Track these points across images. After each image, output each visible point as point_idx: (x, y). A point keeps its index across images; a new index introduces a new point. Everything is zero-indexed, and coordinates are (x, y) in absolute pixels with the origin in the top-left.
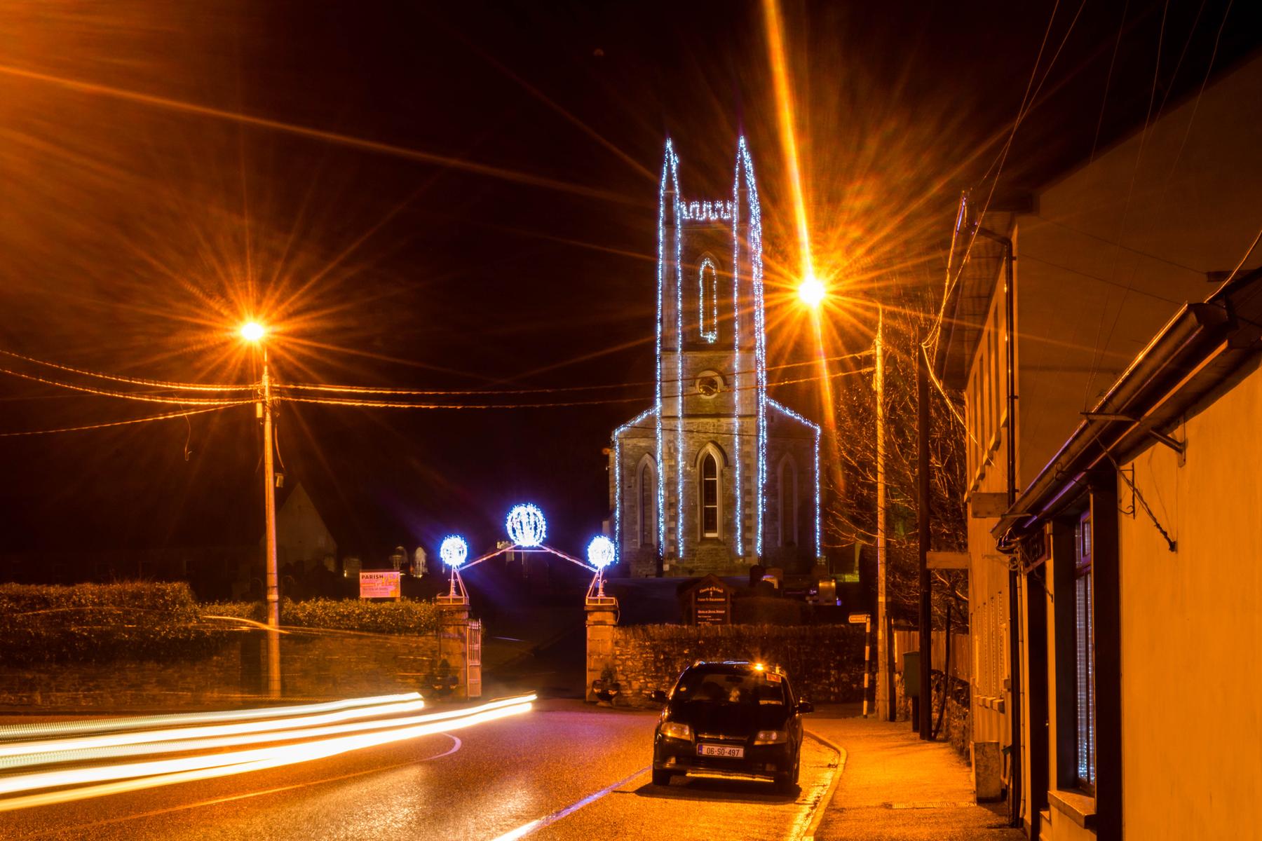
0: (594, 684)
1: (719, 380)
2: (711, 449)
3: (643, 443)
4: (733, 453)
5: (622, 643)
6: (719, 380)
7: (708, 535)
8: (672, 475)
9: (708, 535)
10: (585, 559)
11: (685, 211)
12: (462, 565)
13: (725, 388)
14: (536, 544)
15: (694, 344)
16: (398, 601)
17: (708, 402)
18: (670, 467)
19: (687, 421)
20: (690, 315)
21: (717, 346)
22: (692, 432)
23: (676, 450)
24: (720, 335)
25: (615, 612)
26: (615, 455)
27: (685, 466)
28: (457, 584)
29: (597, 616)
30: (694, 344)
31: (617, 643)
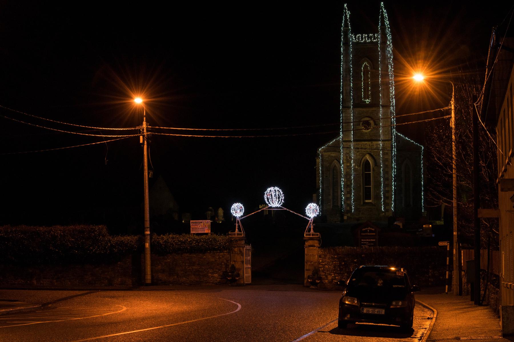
0: (309, 277)
1: (367, 119)
2: (368, 157)
3: (333, 154)
5: (323, 256)
6: (367, 119)
7: (367, 201)
8: (348, 170)
9: (367, 201)
10: (304, 213)
12: (242, 216)
13: (375, 126)
14: (279, 206)
15: (359, 104)
16: (209, 235)
17: (366, 133)
18: (347, 166)
19: (356, 143)
21: (370, 105)
23: (350, 158)
24: (372, 100)
25: (319, 240)
26: (319, 161)
27: (355, 166)
28: (239, 226)
29: (310, 242)
30: (359, 104)
31: (320, 256)
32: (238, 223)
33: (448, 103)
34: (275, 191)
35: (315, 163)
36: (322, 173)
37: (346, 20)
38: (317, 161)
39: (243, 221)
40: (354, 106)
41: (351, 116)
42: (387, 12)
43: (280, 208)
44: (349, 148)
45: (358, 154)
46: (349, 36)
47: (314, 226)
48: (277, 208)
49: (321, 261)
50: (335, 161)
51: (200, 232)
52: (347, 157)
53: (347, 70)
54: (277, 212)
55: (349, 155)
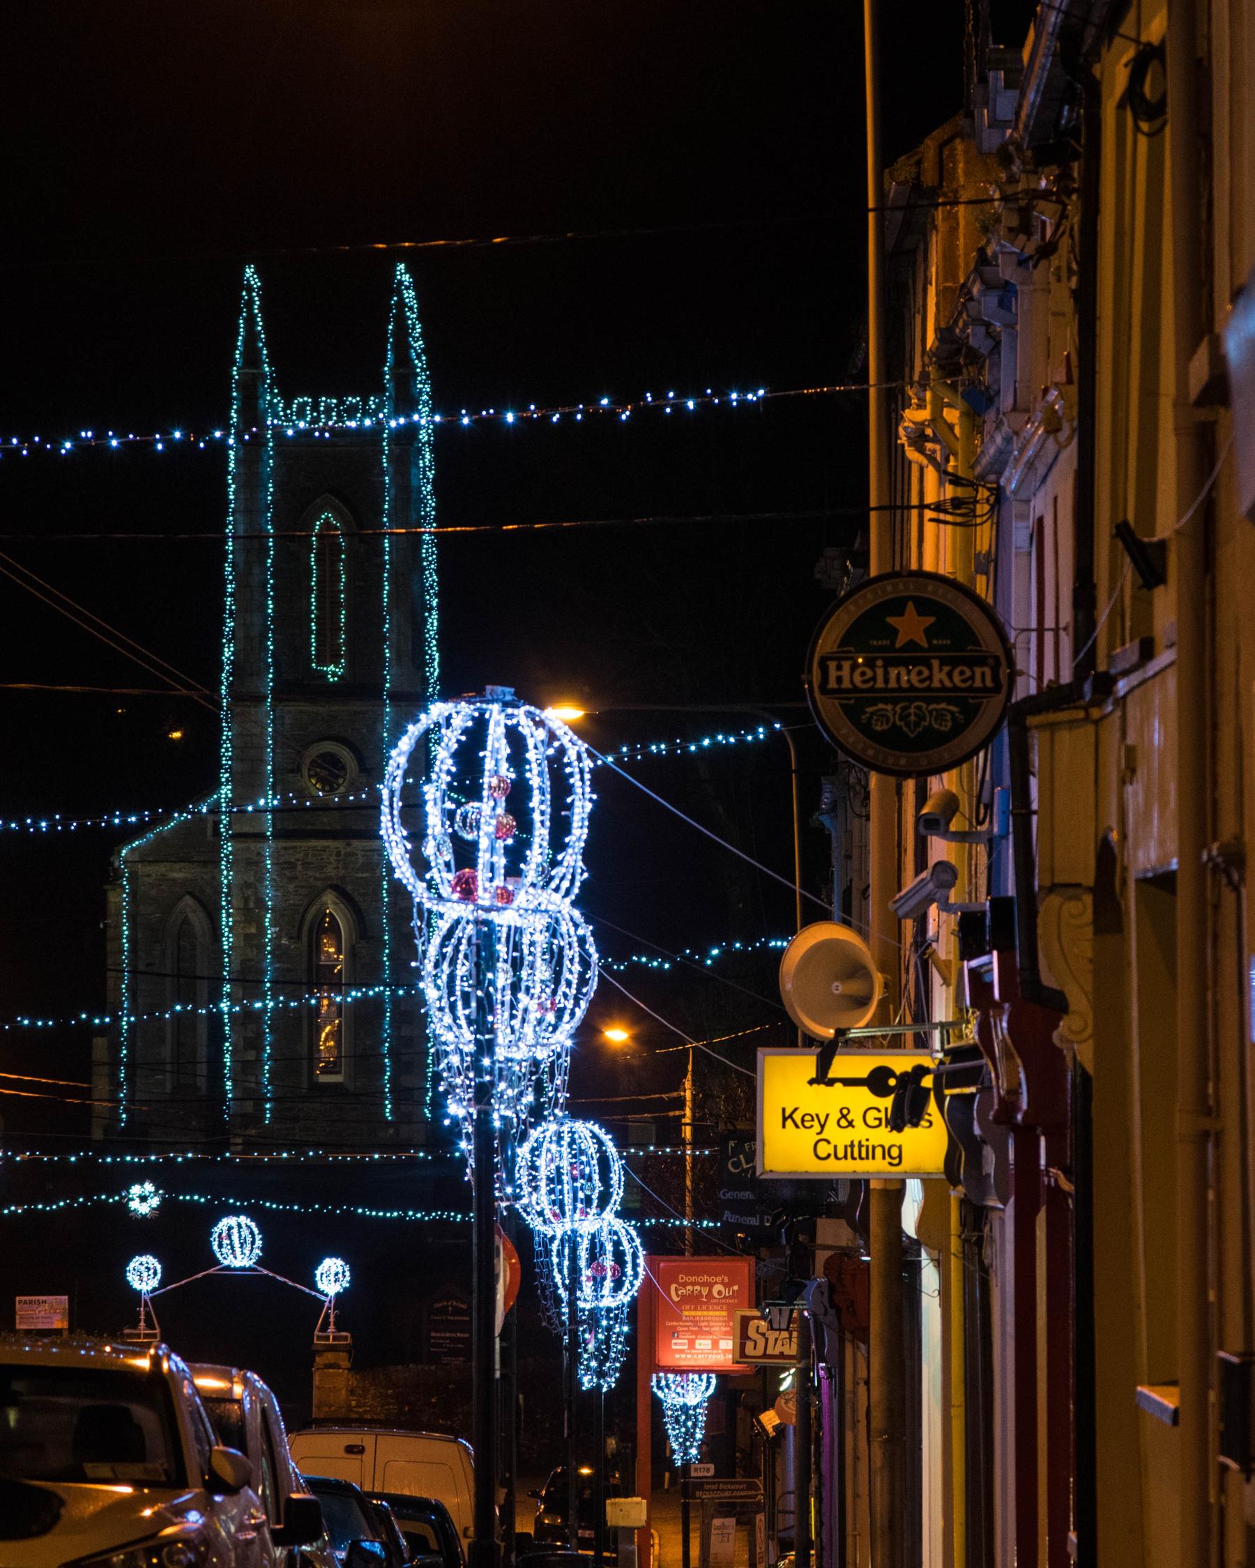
1: (346, 755)
3: (179, 873)
4: (377, 911)
5: (359, 1391)
6: (346, 755)
10: (313, 1286)
11: (292, 419)
12: (154, 1290)
14: (247, 1263)
15: (298, 684)
16: (65, 1334)
18: (248, 937)
19: (282, 844)
20: (291, 620)
21: (349, 689)
22: (292, 866)
23: (261, 903)
24: (350, 668)
25: (349, 1352)
26: (122, 898)
28: (148, 1314)
29: (329, 1357)
30: (298, 684)
31: (352, 1392)
32: (146, 1305)
33: (679, 1085)
34: (239, 1226)
35: (100, 908)
36: (133, 949)
37: (251, 335)
38: (112, 897)
39: (159, 1300)
40: (280, 694)
41: (263, 733)
42: (416, 286)
43: (250, 1269)
44: (257, 863)
45: (291, 887)
46: (263, 405)
47: (336, 1316)
48: (243, 1269)
49: (354, 1403)
50: (188, 899)
51: (40, 1327)
52: (246, 900)
53: (252, 542)
54: (237, 1280)
55: (256, 892)
